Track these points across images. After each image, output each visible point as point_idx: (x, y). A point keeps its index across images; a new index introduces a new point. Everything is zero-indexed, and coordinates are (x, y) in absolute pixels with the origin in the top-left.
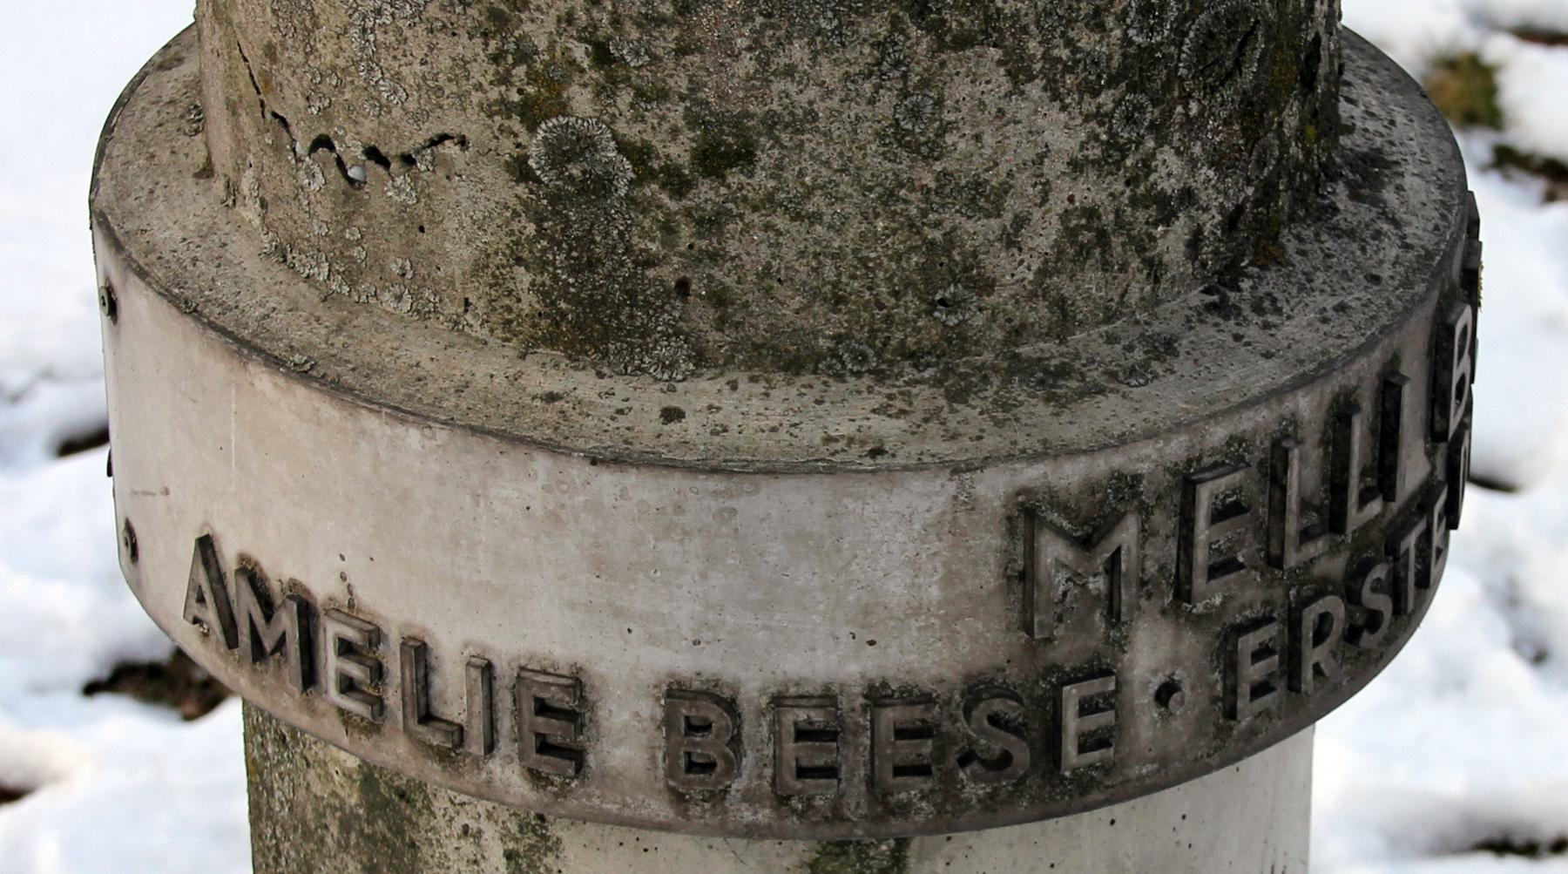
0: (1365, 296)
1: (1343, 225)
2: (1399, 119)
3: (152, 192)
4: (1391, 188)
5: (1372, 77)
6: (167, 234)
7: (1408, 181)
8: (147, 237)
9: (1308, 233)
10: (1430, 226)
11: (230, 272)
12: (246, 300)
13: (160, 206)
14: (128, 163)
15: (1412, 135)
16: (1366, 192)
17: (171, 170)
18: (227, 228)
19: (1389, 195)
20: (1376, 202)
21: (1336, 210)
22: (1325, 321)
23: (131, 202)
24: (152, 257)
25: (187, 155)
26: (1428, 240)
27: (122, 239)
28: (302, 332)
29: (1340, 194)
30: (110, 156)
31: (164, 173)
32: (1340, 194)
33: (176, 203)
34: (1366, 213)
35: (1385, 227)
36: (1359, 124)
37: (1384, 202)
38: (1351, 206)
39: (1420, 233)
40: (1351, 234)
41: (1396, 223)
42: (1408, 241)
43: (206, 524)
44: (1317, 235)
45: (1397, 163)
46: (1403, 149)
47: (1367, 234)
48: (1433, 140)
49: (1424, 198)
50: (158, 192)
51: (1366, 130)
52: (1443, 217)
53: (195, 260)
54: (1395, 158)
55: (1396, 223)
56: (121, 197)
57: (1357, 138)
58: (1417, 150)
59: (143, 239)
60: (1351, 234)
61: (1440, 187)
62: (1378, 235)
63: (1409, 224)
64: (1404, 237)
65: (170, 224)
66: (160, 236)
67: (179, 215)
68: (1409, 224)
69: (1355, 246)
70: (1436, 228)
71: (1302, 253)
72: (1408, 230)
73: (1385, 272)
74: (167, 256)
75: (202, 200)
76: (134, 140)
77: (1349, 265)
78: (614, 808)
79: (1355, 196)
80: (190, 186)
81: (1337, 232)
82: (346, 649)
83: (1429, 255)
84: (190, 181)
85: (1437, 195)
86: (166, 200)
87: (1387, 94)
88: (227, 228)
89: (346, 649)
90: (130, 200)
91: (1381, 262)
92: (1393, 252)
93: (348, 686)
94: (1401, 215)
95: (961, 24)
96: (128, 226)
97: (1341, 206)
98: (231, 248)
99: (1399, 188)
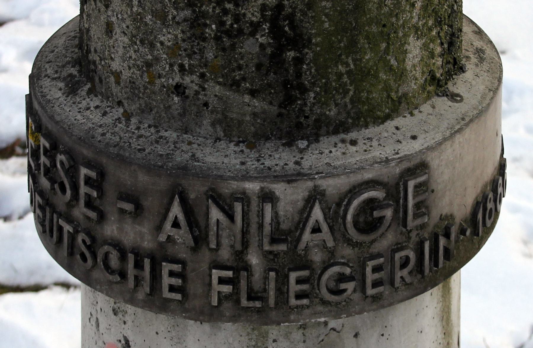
0: (48, 58)
1: (68, 66)
2: (79, 117)
4: (63, 87)
5: (100, 130)
7: (60, 94)
9: (75, 56)
10: (43, 86)
15: (71, 113)
16: (69, 79)
19: (61, 85)
20: (64, 79)
21: (72, 67)
22: (55, 47)
26: (41, 83)
29: (74, 71)
32: (74, 71)
34: (64, 74)
35: (56, 76)
36: (88, 100)
37: (62, 82)
38: (69, 72)
39: (45, 82)
40: (63, 66)
41: (54, 79)
42: (47, 78)
44: (73, 58)
45: (67, 96)
46: (69, 104)
47: (59, 70)
48: (63, 117)
49: (52, 93)
51: (84, 99)
52: (42, 92)
54: (69, 98)
55: (54, 79)
57: (84, 93)
58: (65, 108)
60: (63, 66)
61: (49, 100)
62: (56, 72)
63: (50, 82)
64: (49, 77)
68: (50, 82)
69: (60, 64)
70: (41, 87)
71: (72, 52)
72: (49, 80)
73: (47, 66)
77: (58, 60)
78: (319, 272)
79: (71, 75)
81: (68, 63)
83: (38, 79)
85: (48, 97)
87: (91, 125)
91: (50, 67)
92: (49, 72)
94: (54, 83)
95: (295, 92)
97: (72, 69)
99: (60, 89)
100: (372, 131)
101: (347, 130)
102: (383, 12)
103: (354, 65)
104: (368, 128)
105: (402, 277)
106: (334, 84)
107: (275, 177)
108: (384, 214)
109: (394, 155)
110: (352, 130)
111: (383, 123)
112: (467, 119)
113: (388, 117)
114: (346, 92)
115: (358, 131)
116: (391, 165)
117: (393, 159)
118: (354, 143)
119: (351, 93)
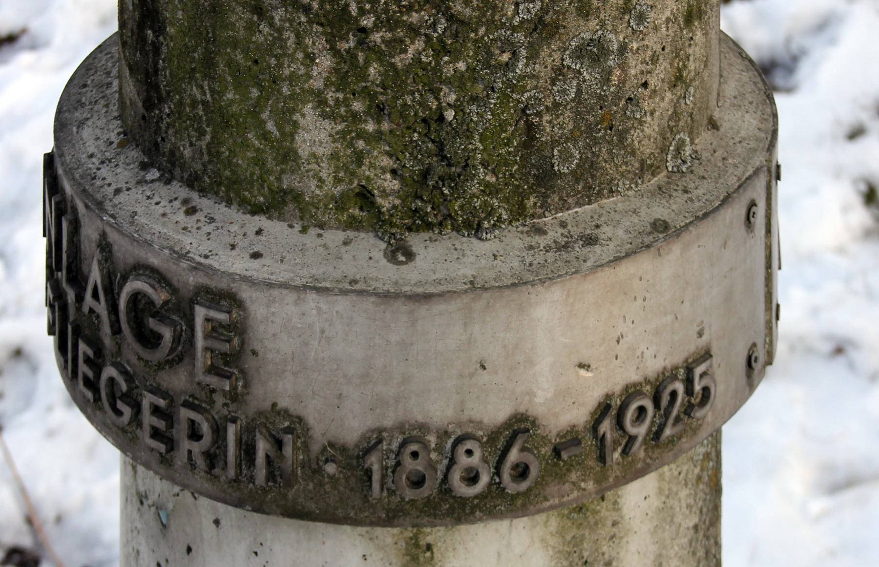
3: (740, 142)
6: (752, 120)
8: (761, 126)
11: (742, 90)
12: (745, 79)
13: (743, 133)
14: (736, 166)
17: (724, 144)
18: (728, 100)
23: (753, 144)
24: (766, 117)
25: (711, 144)
27: (770, 133)
28: (223, 457)
30: (739, 179)
31: (727, 145)
33: (736, 127)
43: (855, 181)
50: (737, 139)
53: (751, 103)
56: (755, 150)
59: (762, 126)
65: (746, 123)
66: (755, 122)
67: (740, 122)
74: (759, 113)
75: (726, 118)
76: (721, 181)
80: (725, 127)
82: (156, 410)
84: (722, 130)
86: (738, 132)
88: (728, 100)
89: (156, 410)
90: (752, 146)
93: (156, 434)
96: (763, 135)
98: (733, 94)
100: (221, 211)
101: (203, 192)
102: (254, 39)
103: (212, 96)
104: (230, 208)
105: (190, 452)
106: (188, 109)
107: (84, 191)
108: (522, 454)
109: (200, 256)
110: (209, 196)
111: (253, 213)
112: (357, 287)
113: (256, 210)
114: (202, 133)
115: (215, 203)
116: (181, 264)
117: (192, 260)
118: (191, 211)
119: (208, 137)
